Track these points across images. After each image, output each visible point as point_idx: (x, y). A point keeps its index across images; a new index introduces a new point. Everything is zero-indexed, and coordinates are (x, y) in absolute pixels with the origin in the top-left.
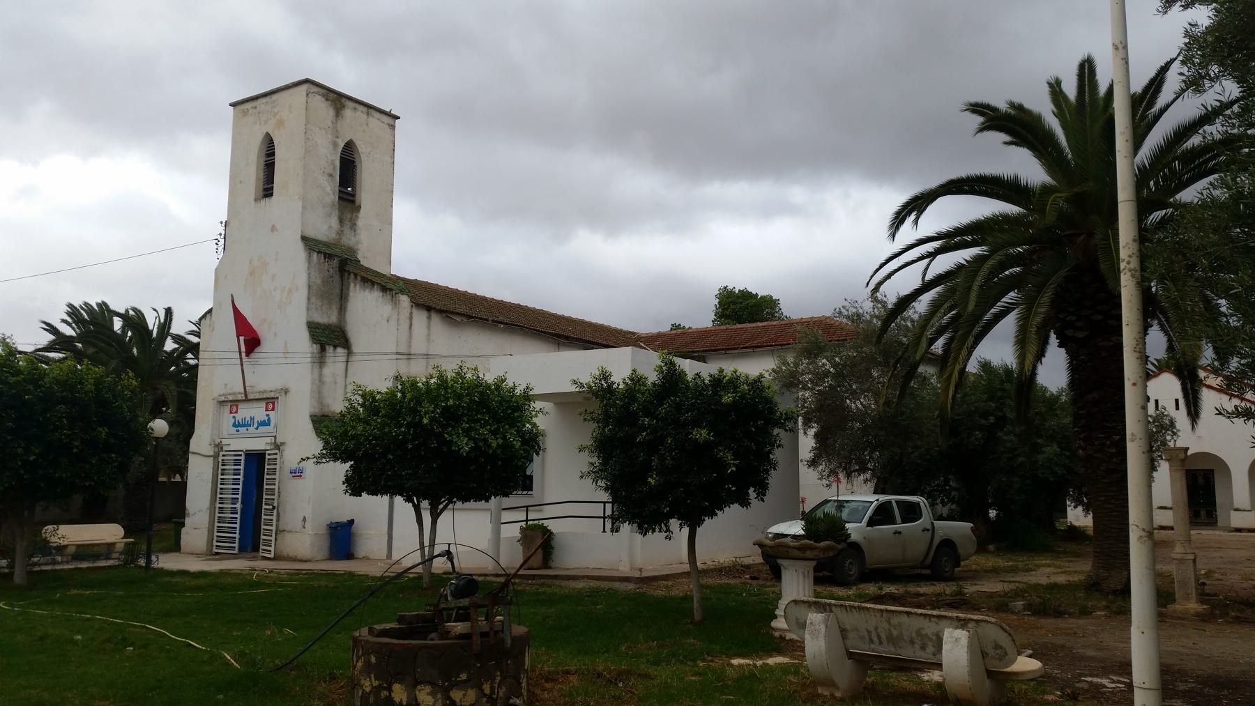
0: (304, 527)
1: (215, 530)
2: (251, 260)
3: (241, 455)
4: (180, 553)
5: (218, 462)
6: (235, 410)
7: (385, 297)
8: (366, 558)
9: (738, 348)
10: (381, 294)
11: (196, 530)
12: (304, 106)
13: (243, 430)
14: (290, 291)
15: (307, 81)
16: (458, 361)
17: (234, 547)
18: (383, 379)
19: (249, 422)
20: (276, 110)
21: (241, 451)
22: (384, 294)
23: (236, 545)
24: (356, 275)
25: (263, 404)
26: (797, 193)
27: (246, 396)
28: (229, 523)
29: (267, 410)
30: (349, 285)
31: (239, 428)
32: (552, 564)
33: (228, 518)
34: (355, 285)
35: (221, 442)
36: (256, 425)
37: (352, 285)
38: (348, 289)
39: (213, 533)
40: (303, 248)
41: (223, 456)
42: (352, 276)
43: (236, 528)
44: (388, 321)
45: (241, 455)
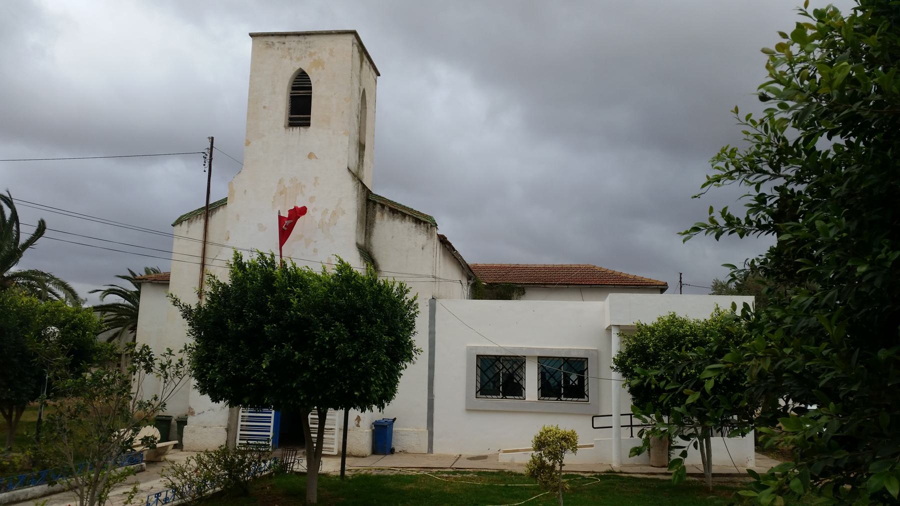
0: (358, 426)
2: (280, 182)
4: (182, 451)
7: (419, 228)
8: (404, 452)
9: (555, 284)
10: (414, 225)
11: (205, 429)
12: (351, 54)
15: (354, 33)
16: (386, 278)
18: (639, 319)
20: (312, 51)
22: (418, 225)
24: (383, 206)
28: (247, 421)
30: (375, 212)
32: (397, 445)
33: (246, 416)
34: (383, 214)
37: (378, 214)
38: (374, 216)
39: (237, 431)
40: (351, 178)
42: (378, 206)
44: (423, 249)
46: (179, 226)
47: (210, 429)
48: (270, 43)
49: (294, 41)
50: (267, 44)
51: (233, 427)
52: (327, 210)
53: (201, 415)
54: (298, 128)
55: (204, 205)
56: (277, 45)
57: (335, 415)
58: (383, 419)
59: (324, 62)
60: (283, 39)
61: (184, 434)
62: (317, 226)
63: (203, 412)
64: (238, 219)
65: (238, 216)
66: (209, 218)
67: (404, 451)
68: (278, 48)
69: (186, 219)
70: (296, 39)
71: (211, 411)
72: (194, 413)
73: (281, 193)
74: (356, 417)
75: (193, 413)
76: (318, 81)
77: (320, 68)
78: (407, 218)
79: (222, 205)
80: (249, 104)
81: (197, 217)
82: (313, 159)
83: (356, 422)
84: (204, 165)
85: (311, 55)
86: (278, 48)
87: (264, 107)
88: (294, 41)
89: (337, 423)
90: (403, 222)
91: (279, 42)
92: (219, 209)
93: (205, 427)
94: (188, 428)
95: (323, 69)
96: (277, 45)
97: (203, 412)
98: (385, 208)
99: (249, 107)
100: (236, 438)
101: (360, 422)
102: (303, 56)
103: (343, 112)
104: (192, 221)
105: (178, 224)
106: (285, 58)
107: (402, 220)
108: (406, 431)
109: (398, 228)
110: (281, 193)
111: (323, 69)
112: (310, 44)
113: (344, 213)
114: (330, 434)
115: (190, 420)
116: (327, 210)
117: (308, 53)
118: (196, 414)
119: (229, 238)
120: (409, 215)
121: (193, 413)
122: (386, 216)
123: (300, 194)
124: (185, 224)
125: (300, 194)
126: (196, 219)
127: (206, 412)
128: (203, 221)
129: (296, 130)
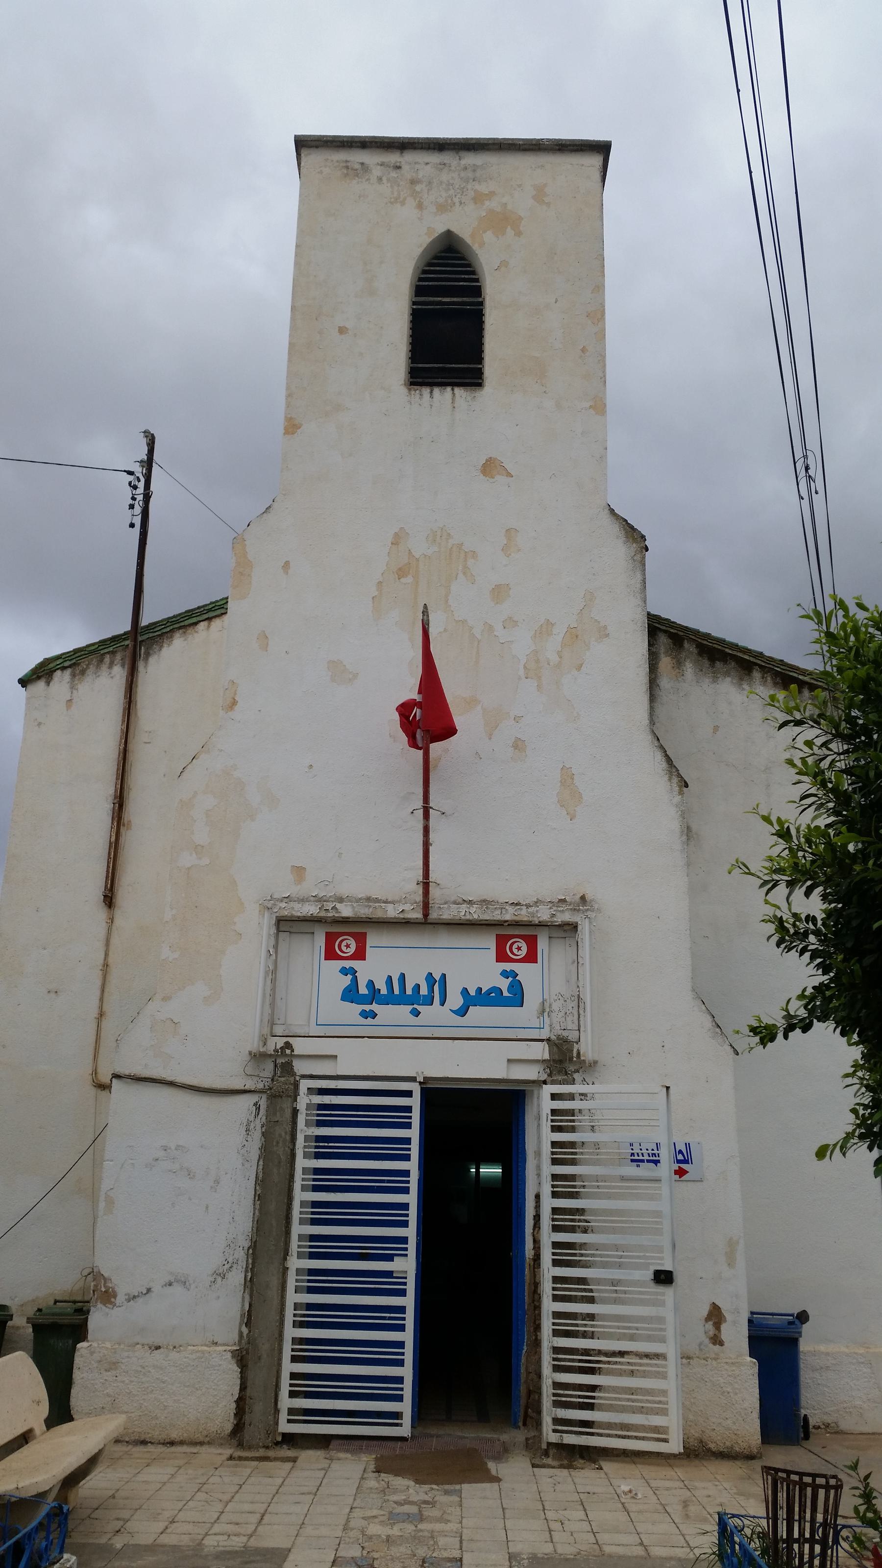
0: (716, 1340)
1: (287, 1354)
2: (397, 540)
3: (408, 1094)
5: (295, 1112)
6: (352, 950)
13: (387, 1013)
14: (573, 636)
17: (397, 1415)
19: (424, 991)
20: (483, 188)
21: (413, 1079)
23: (406, 1407)
25: (490, 942)
26: (130, 763)
27: (426, 915)
29: (502, 957)
31: (375, 1007)
35: (288, 1045)
36: (455, 1000)
39: (280, 1365)
41: (554, 1097)
43: (401, 1344)
45: (408, 1094)
46: (41, 684)
47: (174, 1355)
48: (357, 166)
49: (427, 164)
50: (347, 167)
51: (264, 1347)
52: (549, 624)
53: (140, 1300)
54: (449, 389)
55: (128, 627)
56: (377, 172)
57: (662, 1304)
58: (56, 1302)
59: (520, 218)
60: (393, 157)
61: (77, 1375)
62: (521, 672)
63: (149, 1290)
64: (265, 647)
65: (263, 638)
66: (141, 665)
67: (827, 1426)
68: (380, 179)
69: (67, 664)
70: (434, 158)
71: (177, 1289)
72: (115, 1296)
73: (401, 573)
74: (705, 1311)
75: (108, 1297)
76: (504, 264)
77: (510, 231)
78: (757, 674)
79: (180, 628)
80: (293, 319)
81: (101, 661)
82: (498, 478)
83: (710, 1326)
84: (132, 507)
85: (478, 199)
86: (380, 179)
87: (342, 330)
88: (427, 164)
89: (670, 1333)
90: (745, 686)
91: (382, 164)
92: (172, 637)
93: (158, 1348)
94: (92, 1353)
95: (519, 234)
96: (377, 172)
97: (149, 1290)
98: (686, 645)
99: (293, 328)
100: (277, 1387)
101: (724, 1327)
102: (456, 200)
103: (584, 350)
104: (83, 672)
105: (39, 678)
106: (403, 203)
107: (741, 679)
108: (827, 1354)
109: (730, 703)
110: (401, 573)
111: (519, 234)
112: (474, 171)
113: (603, 633)
114: (620, 1373)
115: (97, 1319)
116: (549, 624)
117: (472, 194)
118: (120, 1298)
119: (234, 703)
120: (761, 667)
121: (108, 1297)
122: (689, 668)
123: (461, 575)
124: (62, 679)
125: (461, 575)
126: (98, 667)
127: (157, 1288)
128: (119, 673)
129: (443, 396)
